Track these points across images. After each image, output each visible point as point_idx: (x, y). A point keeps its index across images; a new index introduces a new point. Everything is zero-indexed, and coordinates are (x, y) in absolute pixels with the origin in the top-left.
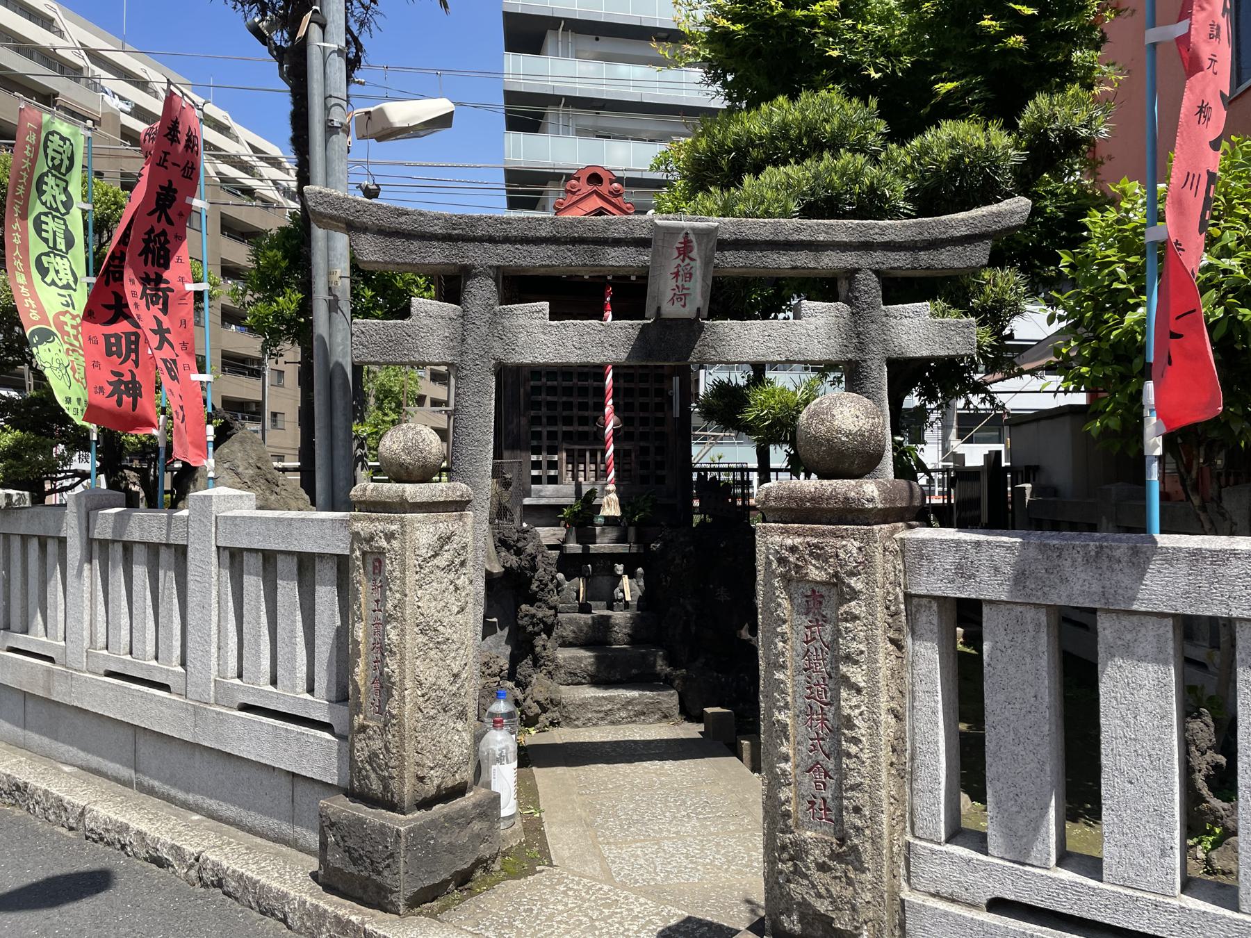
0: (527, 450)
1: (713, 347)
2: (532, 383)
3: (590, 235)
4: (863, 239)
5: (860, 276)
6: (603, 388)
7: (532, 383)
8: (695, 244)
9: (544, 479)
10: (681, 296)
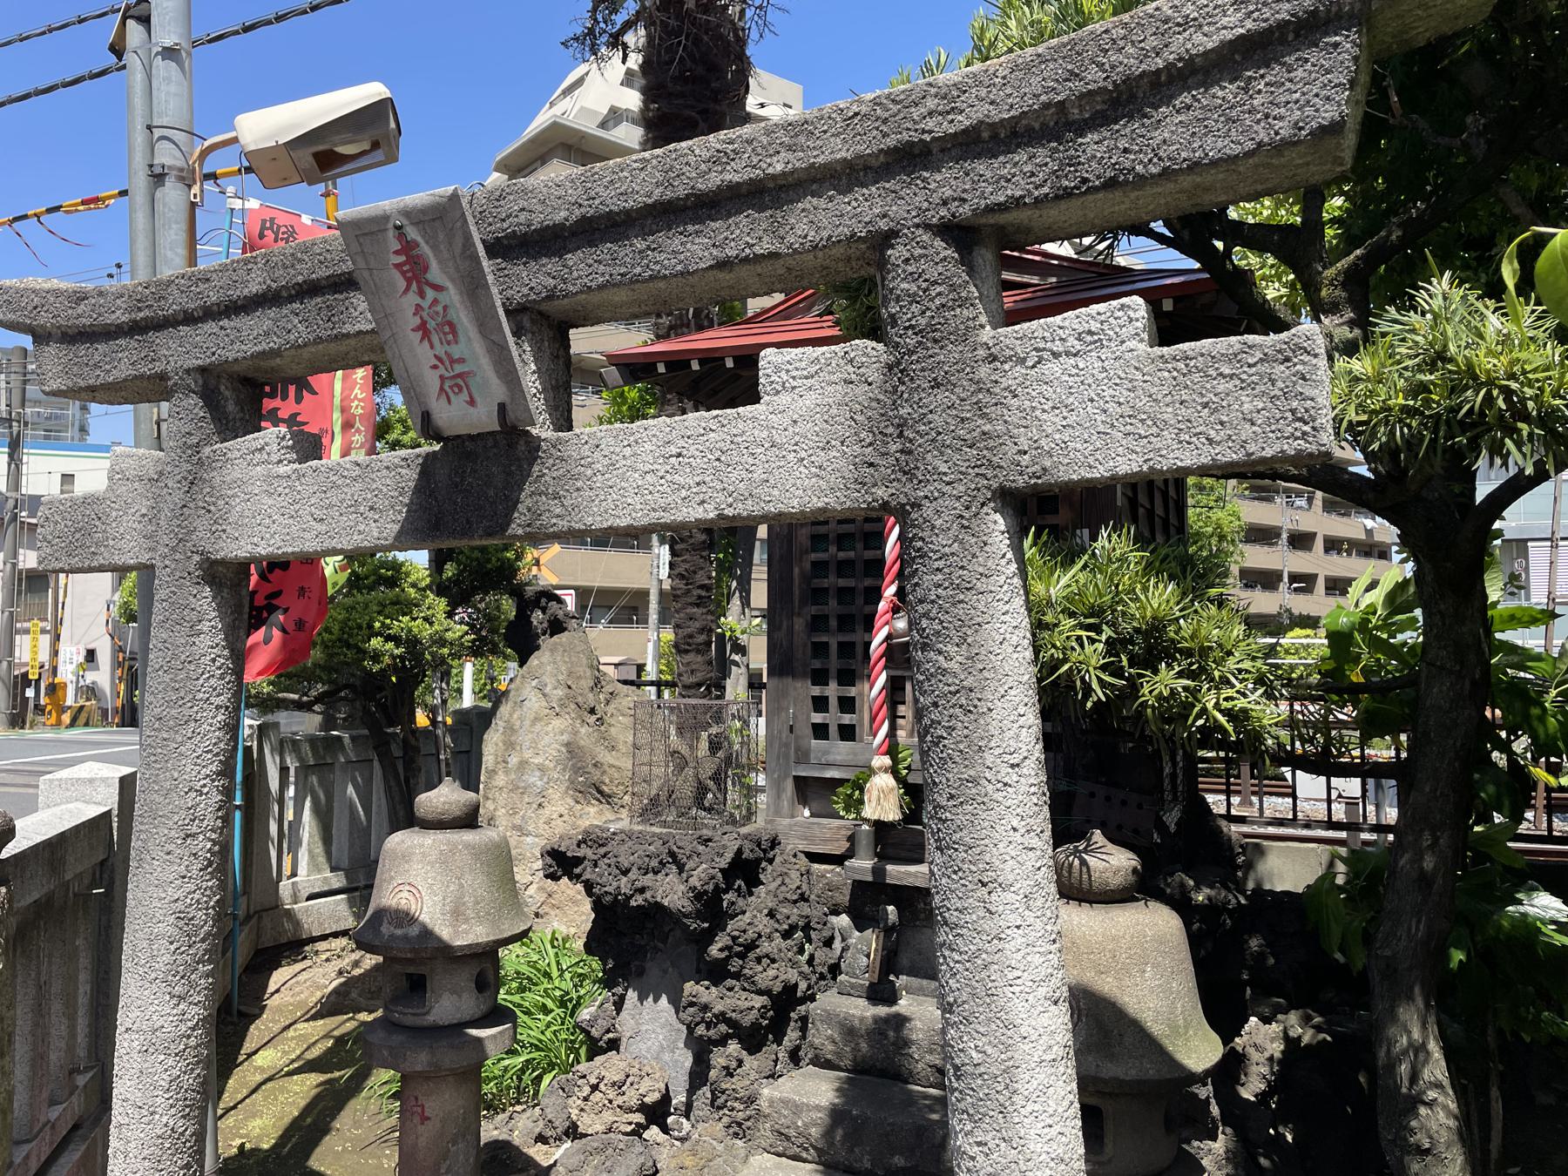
0: (803, 676)
1: (556, 496)
2: (813, 556)
3: (322, 273)
4: (891, 142)
5: (896, 253)
6: (882, 561)
7: (813, 556)
8: (425, 249)
9: (833, 730)
10: (348, 386)
